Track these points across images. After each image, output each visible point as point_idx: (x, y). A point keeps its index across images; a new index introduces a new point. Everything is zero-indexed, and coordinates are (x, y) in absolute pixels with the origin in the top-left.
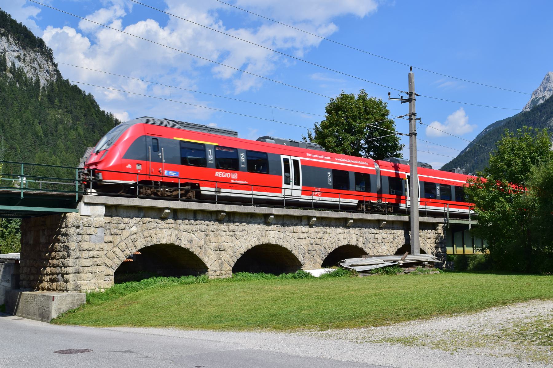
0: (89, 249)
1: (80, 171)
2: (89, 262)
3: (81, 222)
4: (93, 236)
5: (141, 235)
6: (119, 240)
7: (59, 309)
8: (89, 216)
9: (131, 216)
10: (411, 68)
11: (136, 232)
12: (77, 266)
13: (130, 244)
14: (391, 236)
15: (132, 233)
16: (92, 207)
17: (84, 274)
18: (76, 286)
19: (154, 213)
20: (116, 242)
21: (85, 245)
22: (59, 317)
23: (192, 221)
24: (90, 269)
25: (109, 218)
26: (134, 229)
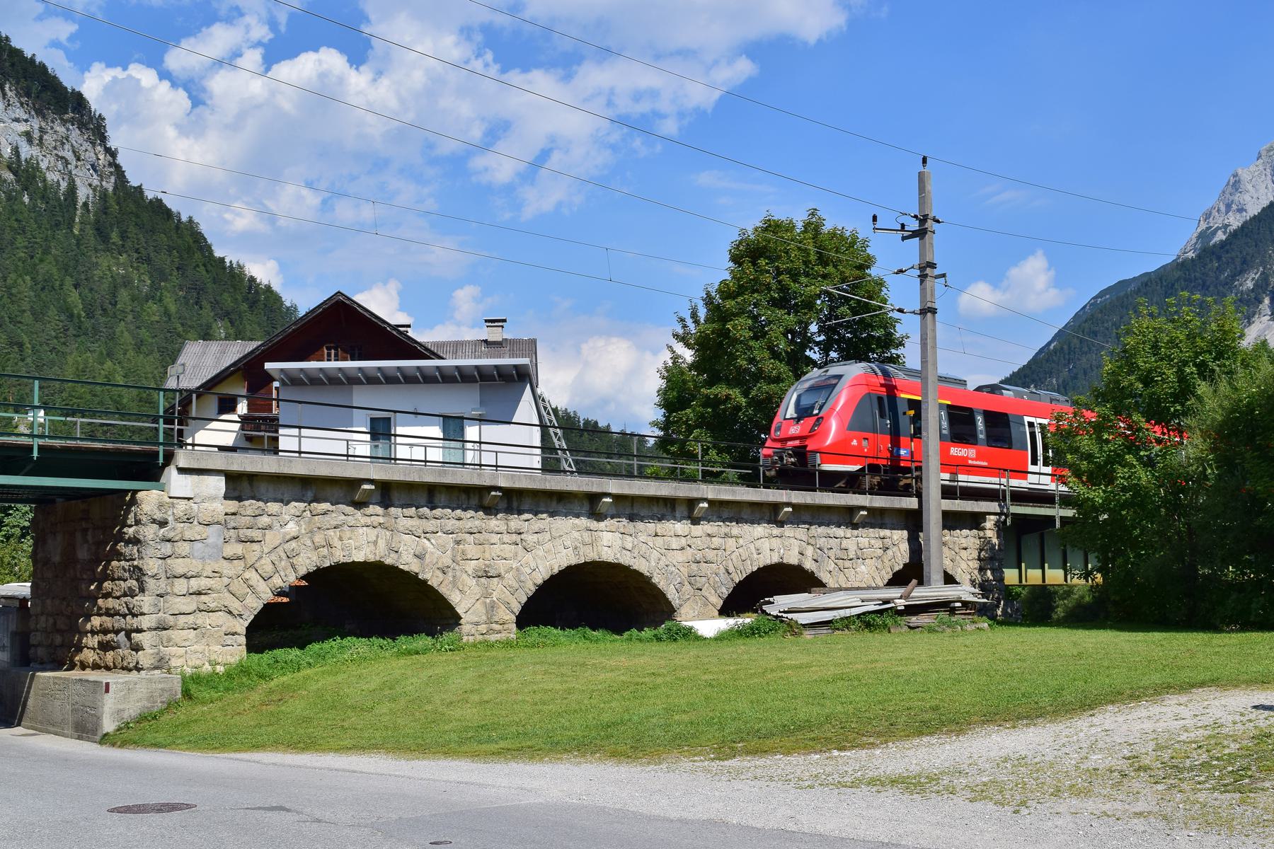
0: (189, 574)
2: (189, 604)
4: (198, 545)
5: (309, 543)
6: (257, 554)
7: (119, 711)
8: (189, 499)
9: (286, 498)
10: (924, 160)
11: (295, 535)
12: (161, 614)
14: (878, 544)
15: (288, 537)
16: (195, 477)
17: (176, 632)
18: (158, 658)
19: (338, 492)
21: (179, 566)
22: (119, 729)
23: (425, 510)
24: (191, 619)
26: (292, 528)
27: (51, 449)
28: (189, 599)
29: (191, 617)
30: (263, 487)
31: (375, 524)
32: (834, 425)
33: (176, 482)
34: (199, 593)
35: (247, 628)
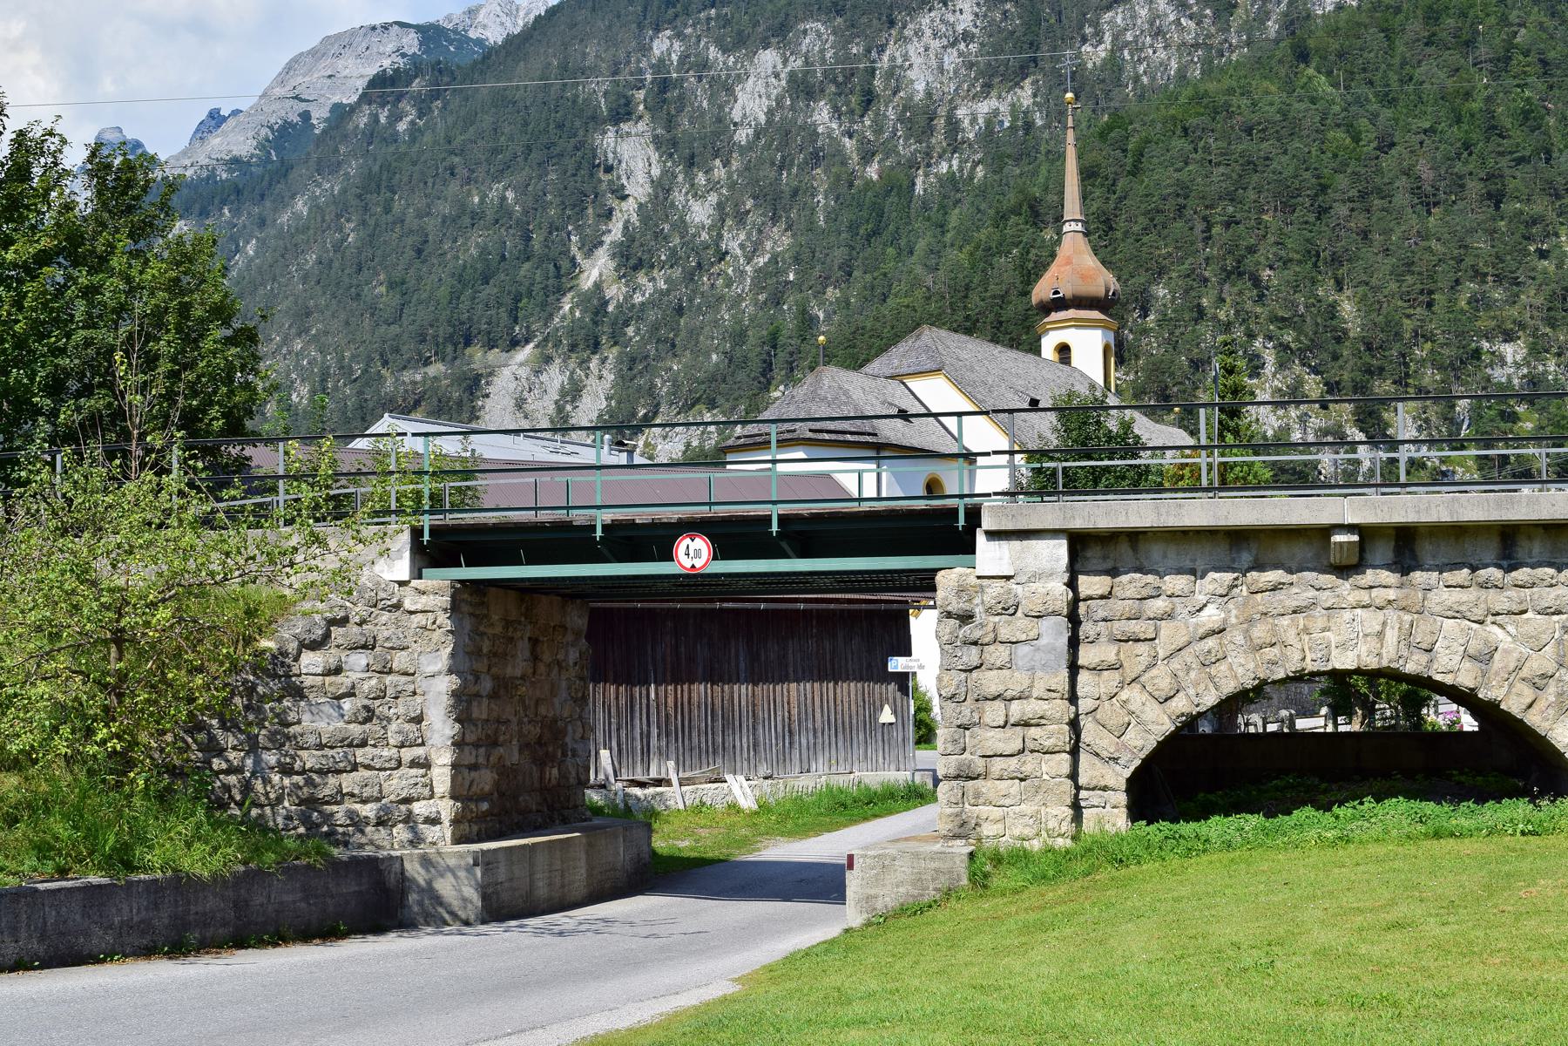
0: (1009, 694)
1: (474, 425)
2: (1010, 741)
3: (977, 601)
4: (1023, 650)
5: (1239, 639)
6: (1145, 660)
7: (868, 898)
8: (1008, 578)
9: (1200, 567)
11: (1216, 627)
12: (966, 755)
13: (1193, 674)
15: (1201, 631)
16: (1016, 544)
17: (989, 783)
18: (958, 821)
19: (1301, 551)
20: (1131, 670)
21: (991, 682)
22: (869, 924)
23: (1494, 573)
24: (1013, 763)
25: (1107, 580)
26: (1212, 615)
27: (797, 518)
28: (1009, 731)
29: (1014, 760)
30: (1156, 551)
31: (1379, 602)
32: (301, 205)
33: (990, 556)
34: (1027, 724)
35: (1129, 780)
